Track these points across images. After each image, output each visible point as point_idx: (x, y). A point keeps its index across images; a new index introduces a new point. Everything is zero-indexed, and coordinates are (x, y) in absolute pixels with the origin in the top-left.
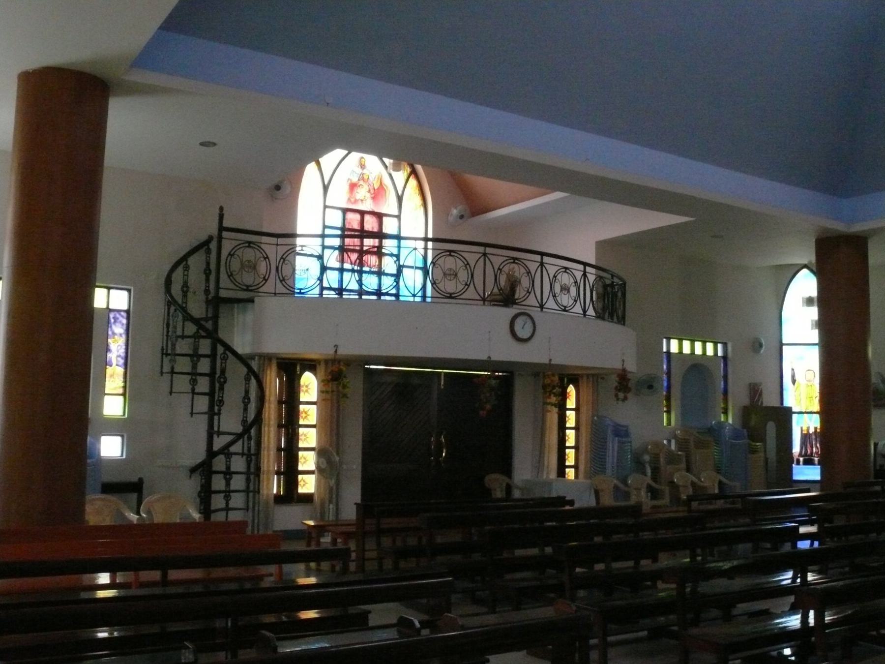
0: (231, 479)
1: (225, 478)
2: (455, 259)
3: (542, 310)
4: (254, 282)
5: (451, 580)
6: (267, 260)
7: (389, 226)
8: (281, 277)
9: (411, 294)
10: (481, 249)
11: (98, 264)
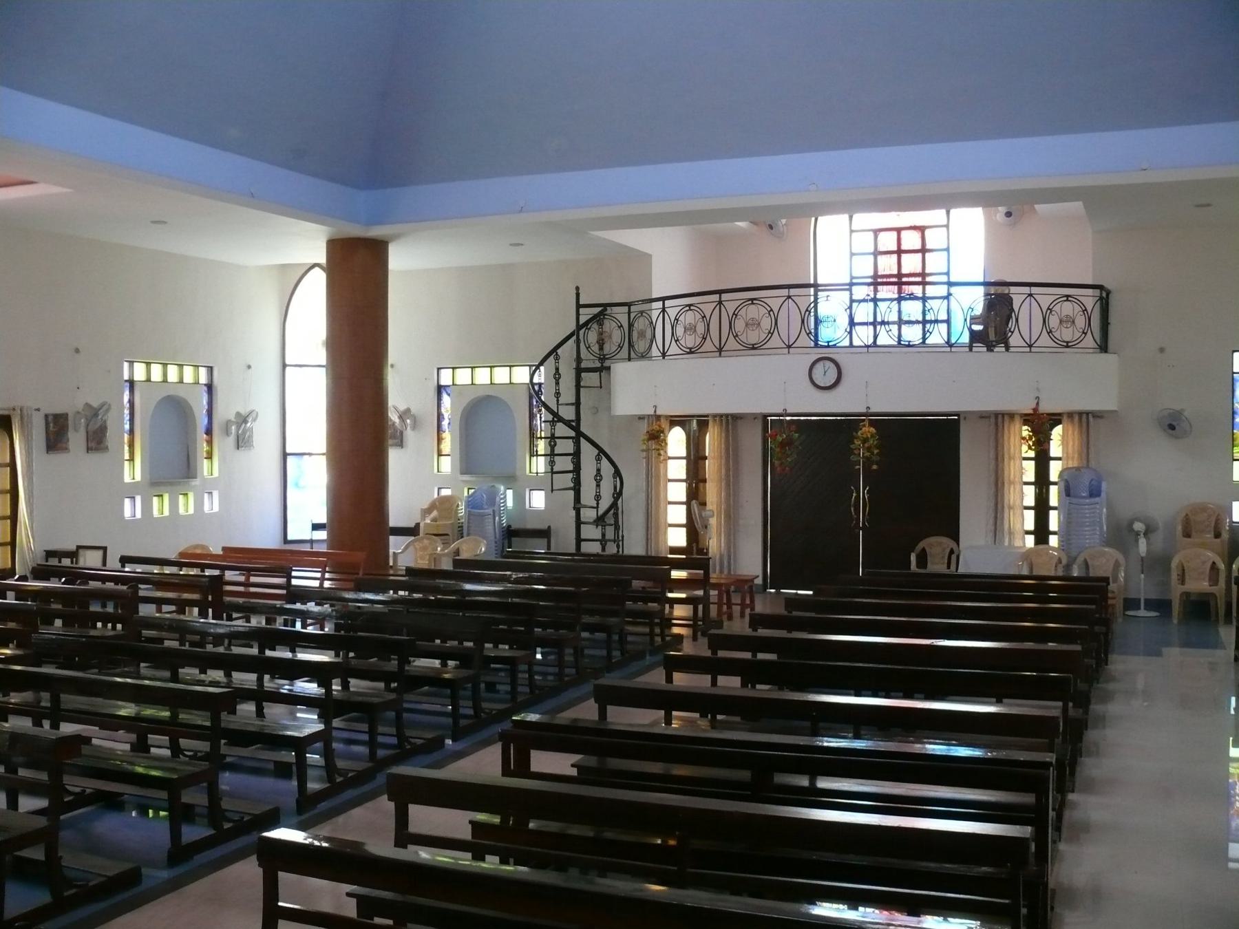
0: (606, 544)
1: (601, 544)
2: (1073, 306)
3: (664, 358)
4: (1073, 338)
5: (683, 558)
6: (736, 313)
7: (935, 263)
8: (807, 330)
9: (1027, 343)
10: (716, 297)
11: (1099, 321)
